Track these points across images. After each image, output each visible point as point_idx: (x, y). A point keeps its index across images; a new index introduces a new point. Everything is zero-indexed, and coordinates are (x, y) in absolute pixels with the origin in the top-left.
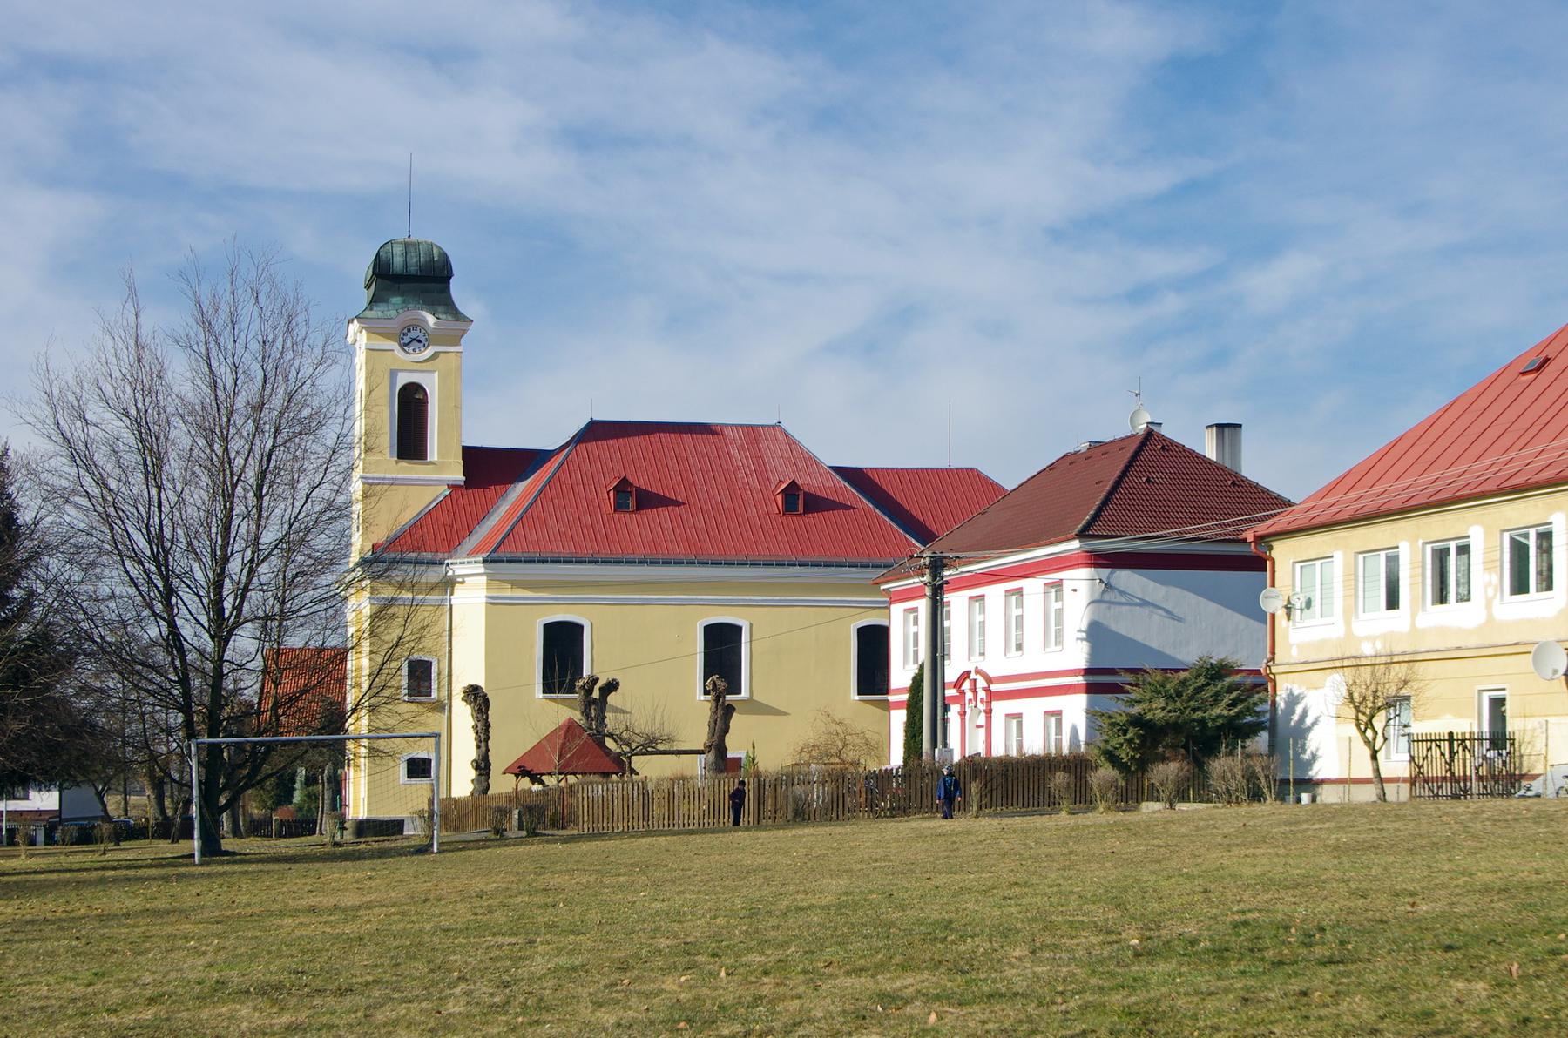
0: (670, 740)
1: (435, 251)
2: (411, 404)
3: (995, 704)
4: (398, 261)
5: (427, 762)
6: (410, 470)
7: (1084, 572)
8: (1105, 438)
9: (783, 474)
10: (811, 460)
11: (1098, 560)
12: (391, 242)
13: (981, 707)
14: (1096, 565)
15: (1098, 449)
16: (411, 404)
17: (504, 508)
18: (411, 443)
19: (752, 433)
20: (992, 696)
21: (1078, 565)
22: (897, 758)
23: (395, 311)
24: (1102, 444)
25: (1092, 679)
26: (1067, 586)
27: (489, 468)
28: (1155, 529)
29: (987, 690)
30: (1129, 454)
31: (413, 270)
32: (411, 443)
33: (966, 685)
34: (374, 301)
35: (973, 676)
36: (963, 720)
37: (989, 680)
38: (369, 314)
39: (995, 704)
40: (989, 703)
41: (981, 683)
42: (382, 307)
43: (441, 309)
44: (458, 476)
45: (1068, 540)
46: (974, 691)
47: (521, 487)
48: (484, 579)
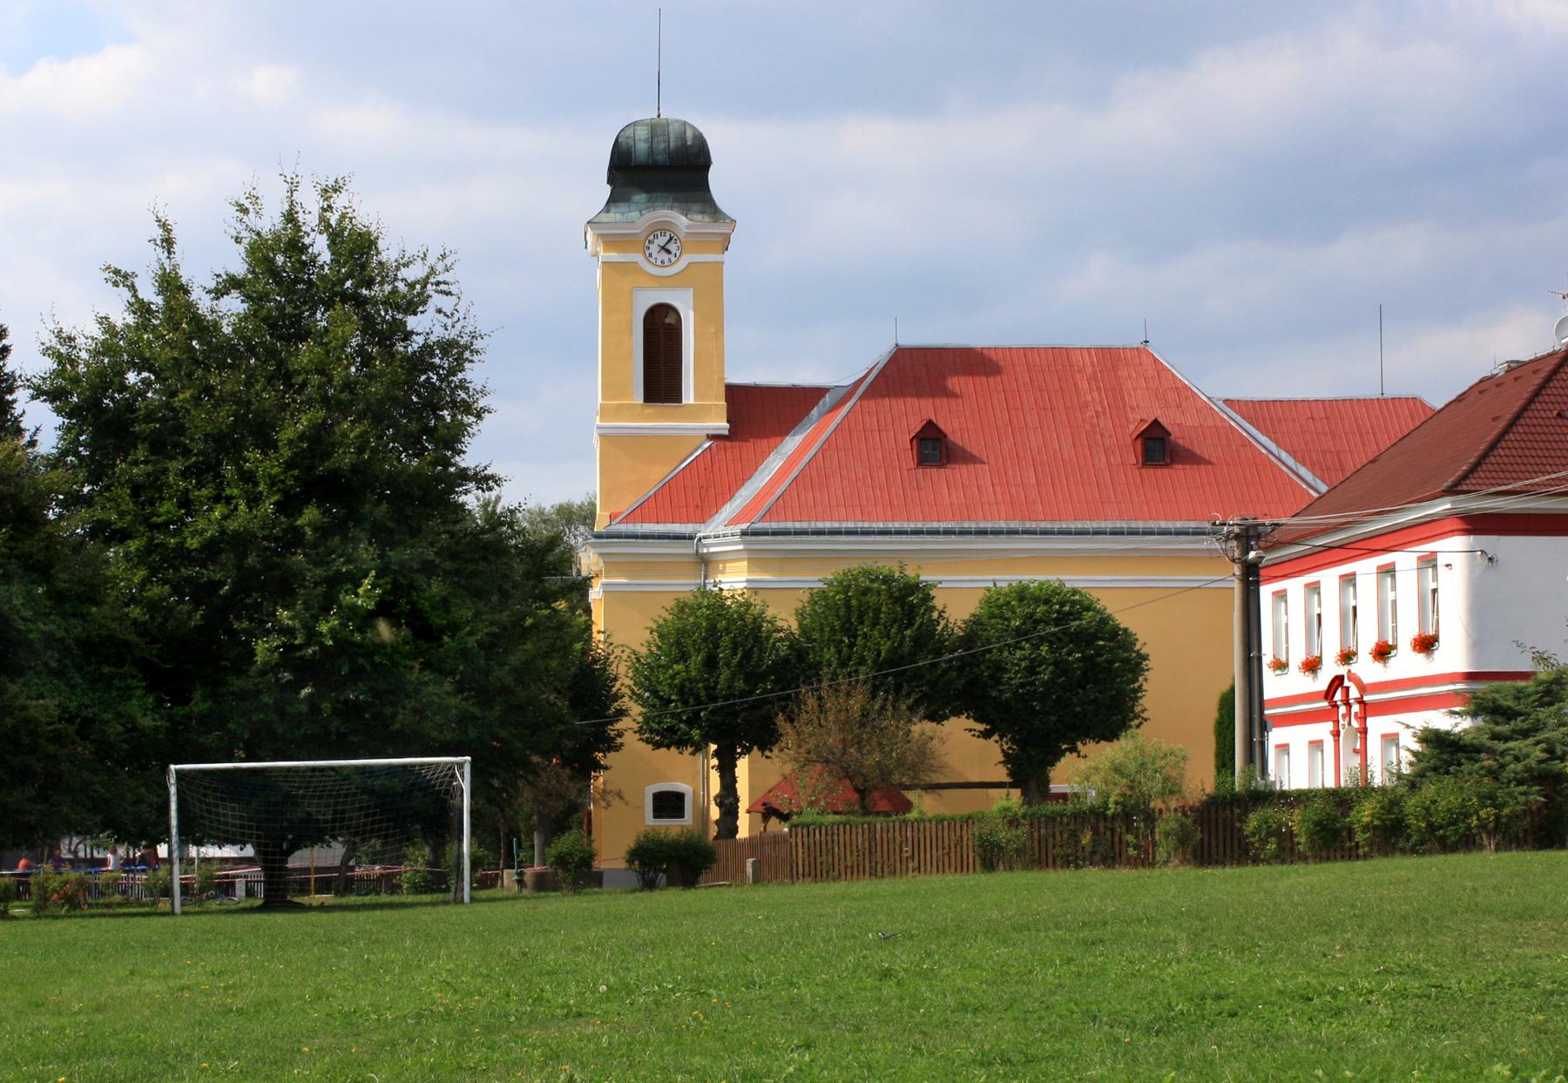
0: (914, 767)
1: (689, 134)
2: (661, 332)
3: (1372, 722)
4: (642, 147)
5: (679, 797)
6: (660, 421)
7: (1459, 542)
8: (1525, 355)
9: (1144, 411)
10: (1183, 392)
11: (1476, 524)
12: (635, 124)
13: (1355, 724)
14: (1467, 532)
15: (1516, 369)
16: (661, 332)
17: (774, 463)
18: (662, 381)
19: (1109, 358)
20: (1367, 709)
21: (1452, 532)
22: (742, 767)
23: (640, 216)
24: (1522, 364)
25: (1481, 687)
26: (1442, 560)
27: (759, 412)
28: (1509, 480)
29: (1360, 701)
30: (1538, 379)
31: (660, 158)
32: (662, 381)
33: (1338, 696)
34: (612, 200)
35: (1346, 683)
36: (1337, 742)
37: (1363, 688)
38: (604, 218)
39: (1370, 721)
40: (1363, 718)
41: (1354, 693)
42: (623, 207)
43: (697, 207)
44: (721, 425)
45: (1435, 497)
46: (1348, 705)
47: (792, 443)
48: (745, 563)
